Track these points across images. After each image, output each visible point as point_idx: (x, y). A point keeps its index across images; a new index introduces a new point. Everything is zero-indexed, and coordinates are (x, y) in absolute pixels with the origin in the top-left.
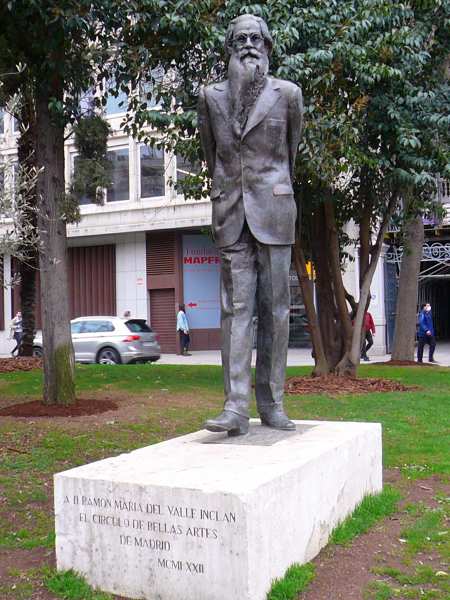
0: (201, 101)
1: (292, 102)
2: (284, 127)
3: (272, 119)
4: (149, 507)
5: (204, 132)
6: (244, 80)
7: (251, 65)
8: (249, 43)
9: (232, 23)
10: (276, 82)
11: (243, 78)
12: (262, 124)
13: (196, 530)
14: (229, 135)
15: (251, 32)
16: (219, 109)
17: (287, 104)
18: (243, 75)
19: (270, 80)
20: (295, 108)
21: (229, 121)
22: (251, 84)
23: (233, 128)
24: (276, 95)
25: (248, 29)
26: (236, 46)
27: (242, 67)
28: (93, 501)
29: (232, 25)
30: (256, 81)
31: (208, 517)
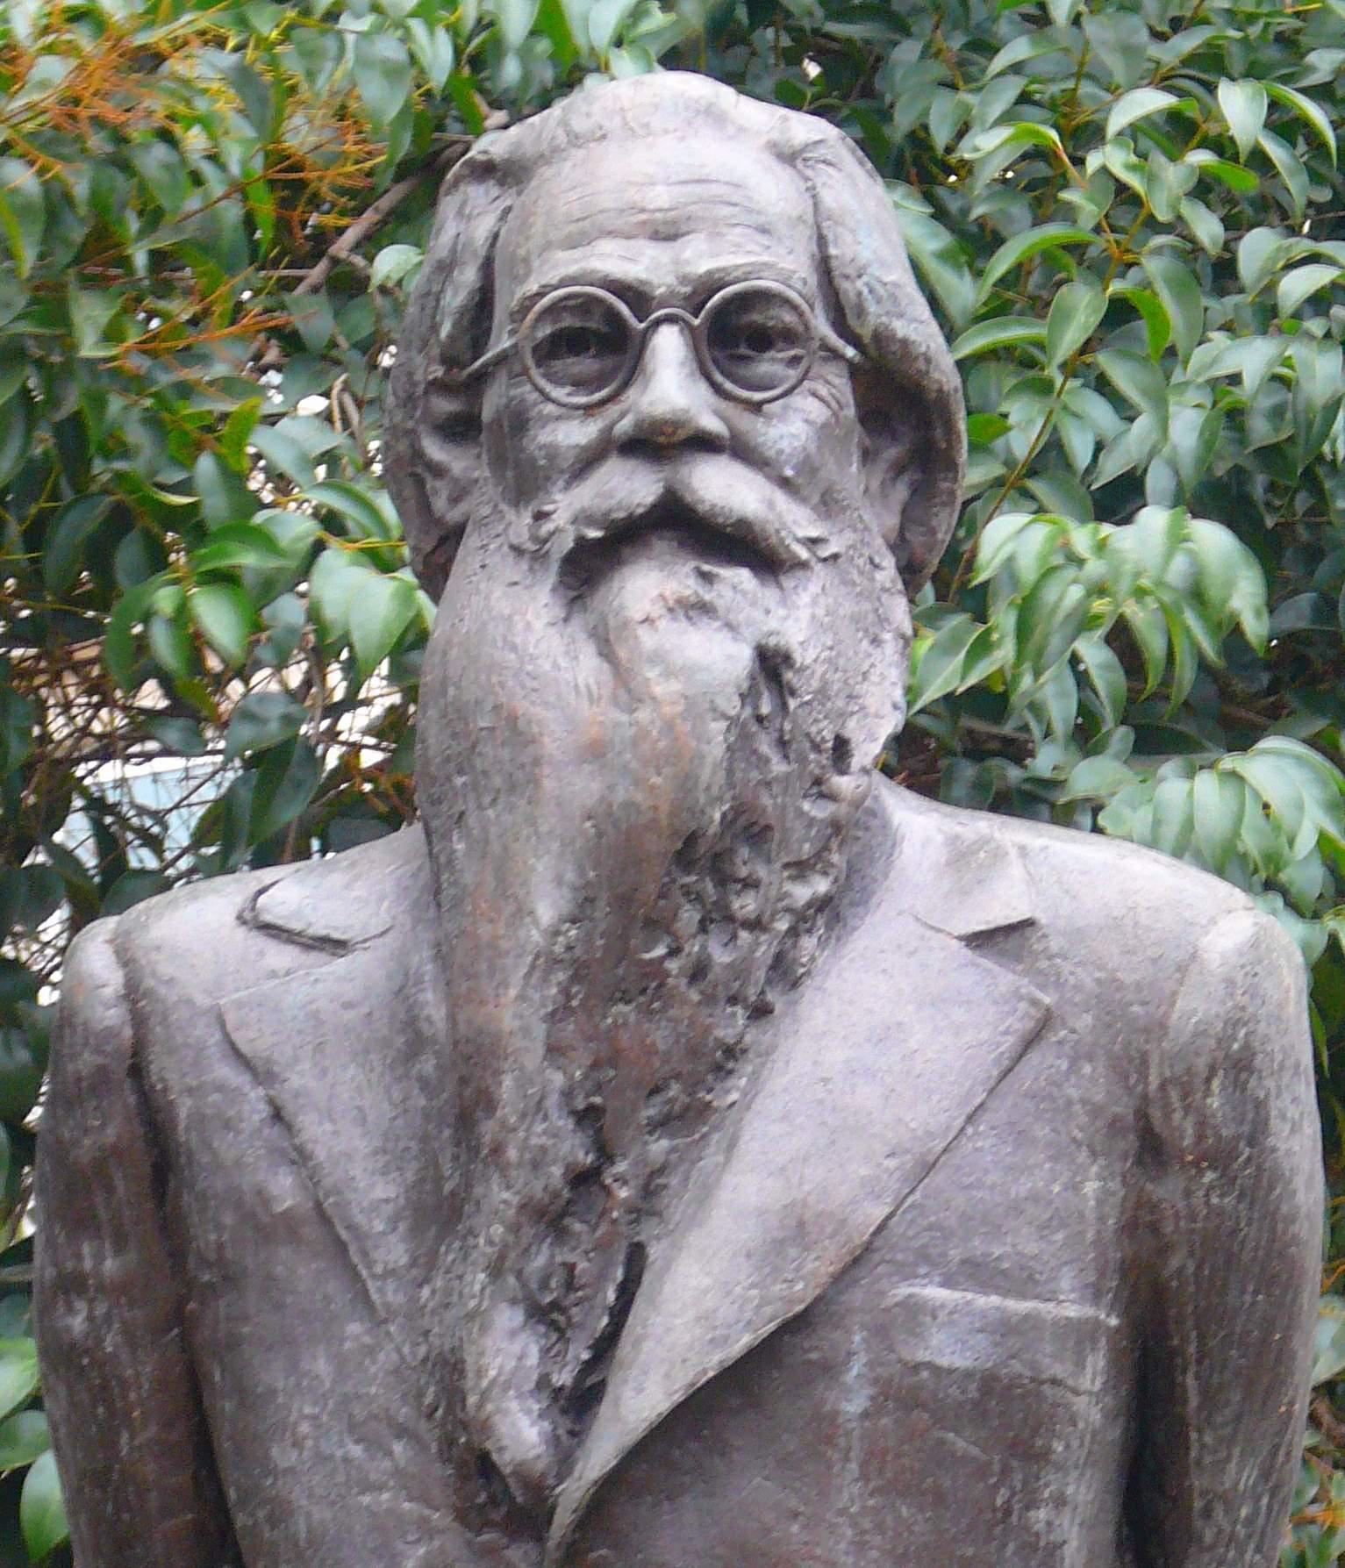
0: (87, 1061)
1: (1187, 1086)
2: (1088, 1392)
3: (934, 1293)
5: (109, 1444)
6: (601, 815)
7: (688, 639)
8: (670, 381)
9: (486, 170)
10: (998, 855)
11: (585, 787)
12: (814, 1348)
15: (703, 267)
16: (300, 1158)
17: (1124, 1108)
18: (595, 752)
19: (919, 826)
20: (1219, 1157)
21: (415, 1311)
22: (686, 856)
23: (453, 1394)
24: (987, 1005)
25: (667, 232)
26: (518, 421)
27: (588, 667)
29: (479, 195)
30: (751, 829)
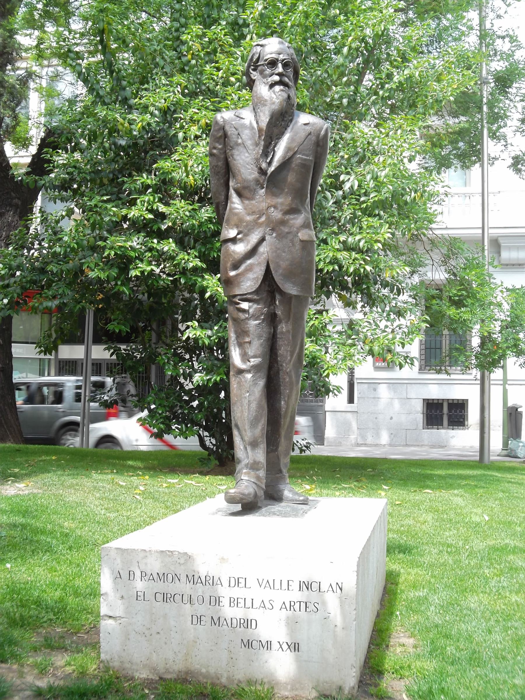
4: (232, 580)
13: (292, 604)
14: (252, 169)
28: (155, 576)
31: (308, 588)
